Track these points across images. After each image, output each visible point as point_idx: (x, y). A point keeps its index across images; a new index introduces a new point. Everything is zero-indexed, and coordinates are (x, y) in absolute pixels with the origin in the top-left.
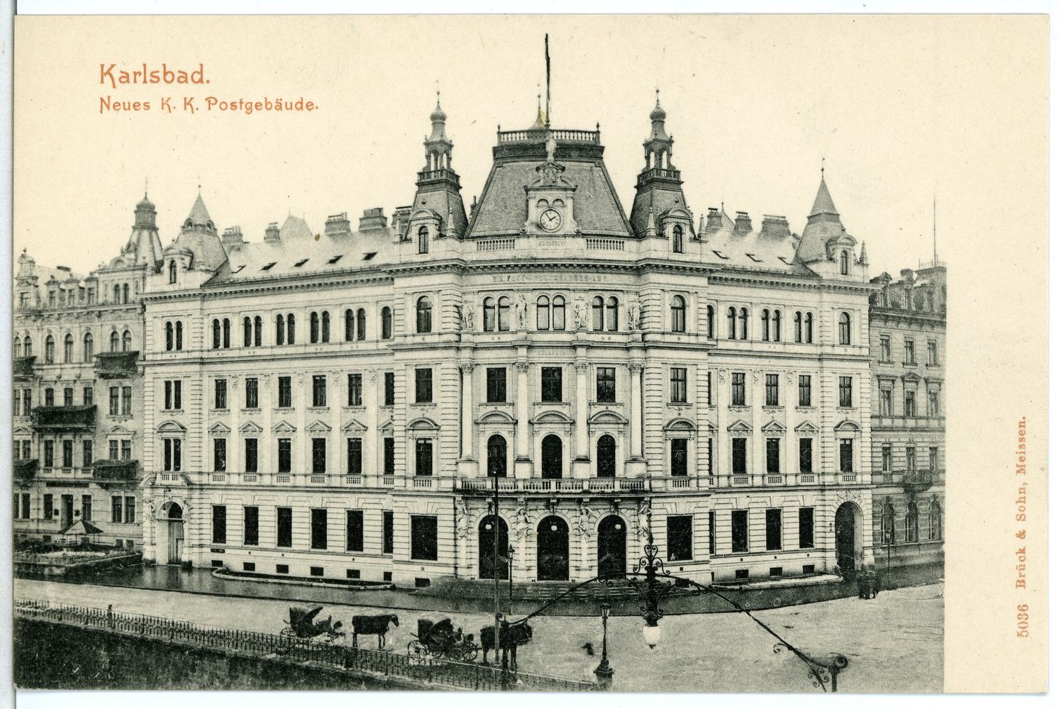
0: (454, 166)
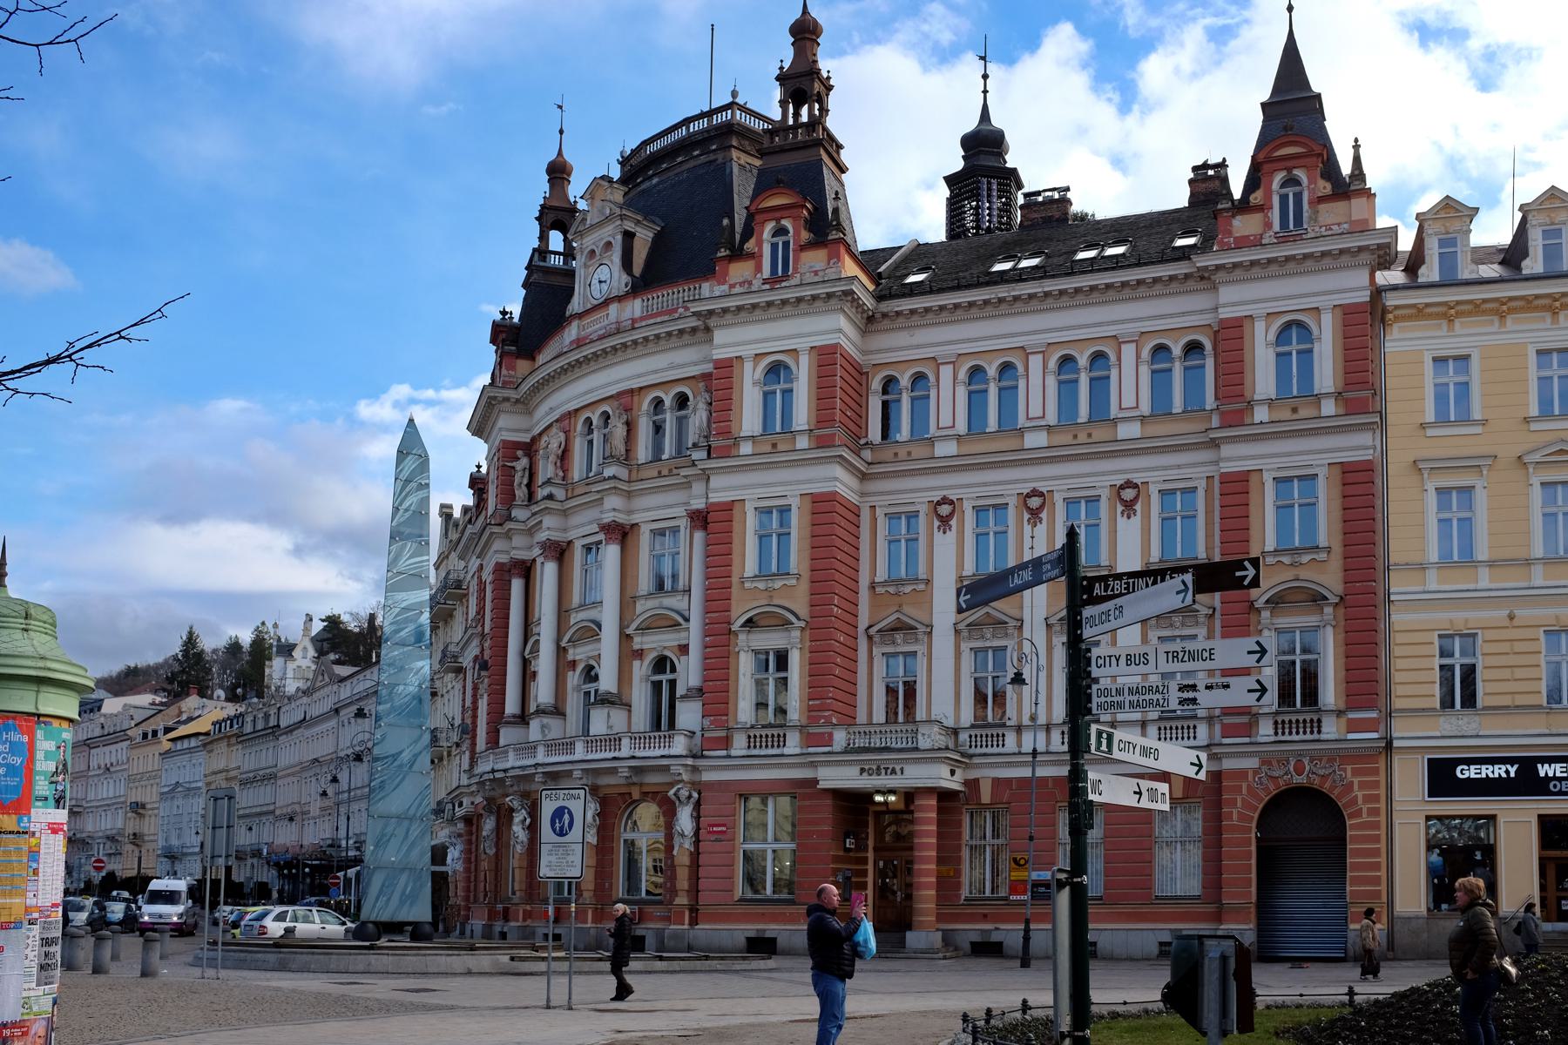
0: (831, 123)
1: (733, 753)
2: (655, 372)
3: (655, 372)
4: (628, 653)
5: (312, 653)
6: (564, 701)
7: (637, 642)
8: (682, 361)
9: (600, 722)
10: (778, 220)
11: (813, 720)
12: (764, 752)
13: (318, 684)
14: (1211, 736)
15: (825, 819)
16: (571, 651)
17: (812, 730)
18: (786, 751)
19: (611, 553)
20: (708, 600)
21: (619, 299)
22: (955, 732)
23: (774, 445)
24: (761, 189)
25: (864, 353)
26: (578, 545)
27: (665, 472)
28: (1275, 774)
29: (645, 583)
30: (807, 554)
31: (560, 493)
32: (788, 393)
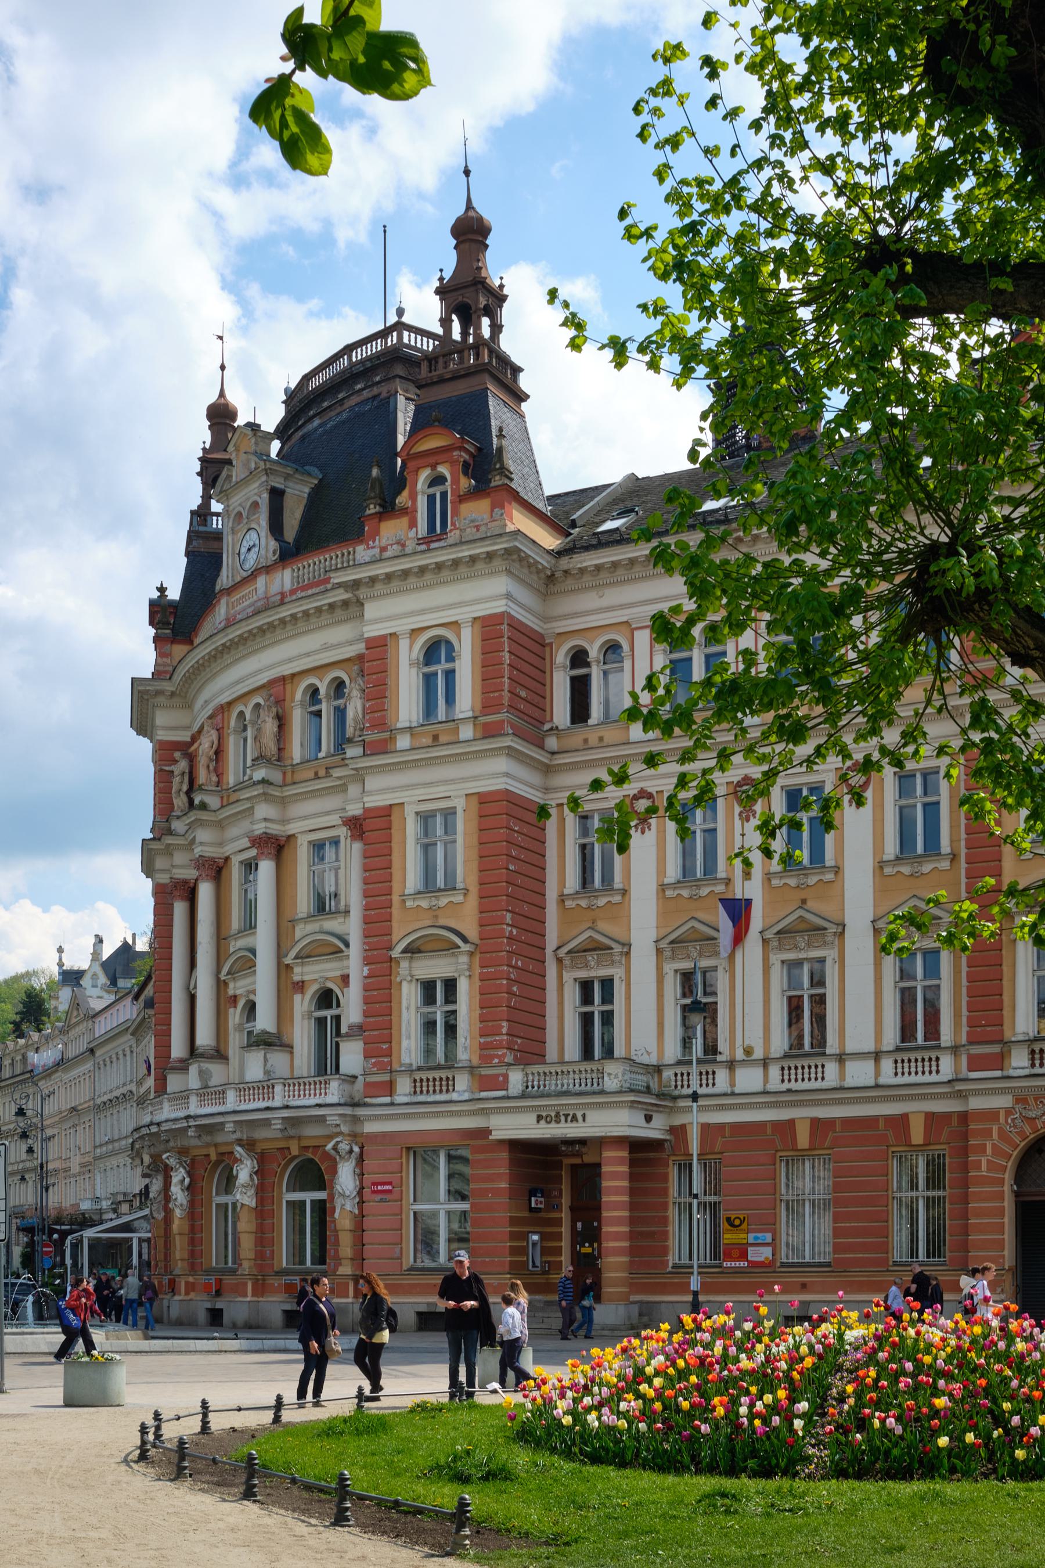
0: (507, 344)
1: (399, 1099)
2: (308, 655)
3: (308, 655)
4: (287, 985)
5: (103, 979)
6: (226, 1042)
7: (298, 973)
8: (329, 643)
9: (254, 1066)
10: (434, 467)
11: (486, 1059)
12: (431, 1098)
13: (74, 1020)
14: (957, 1071)
15: (497, 1177)
16: (231, 985)
17: (484, 1072)
18: (455, 1096)
19: (266, 868)
20: (367, 921)
21: (267, 569)
22: (658, 1069)
23: (436, 738)
24: (418, 426)
25: (546, 619)
26: (235, 861)
27: (322, 773)
28: (1032, 1114)
29: (304, 904)
30: (474, 866)
31: (213, 802)
32: (450, 674)
